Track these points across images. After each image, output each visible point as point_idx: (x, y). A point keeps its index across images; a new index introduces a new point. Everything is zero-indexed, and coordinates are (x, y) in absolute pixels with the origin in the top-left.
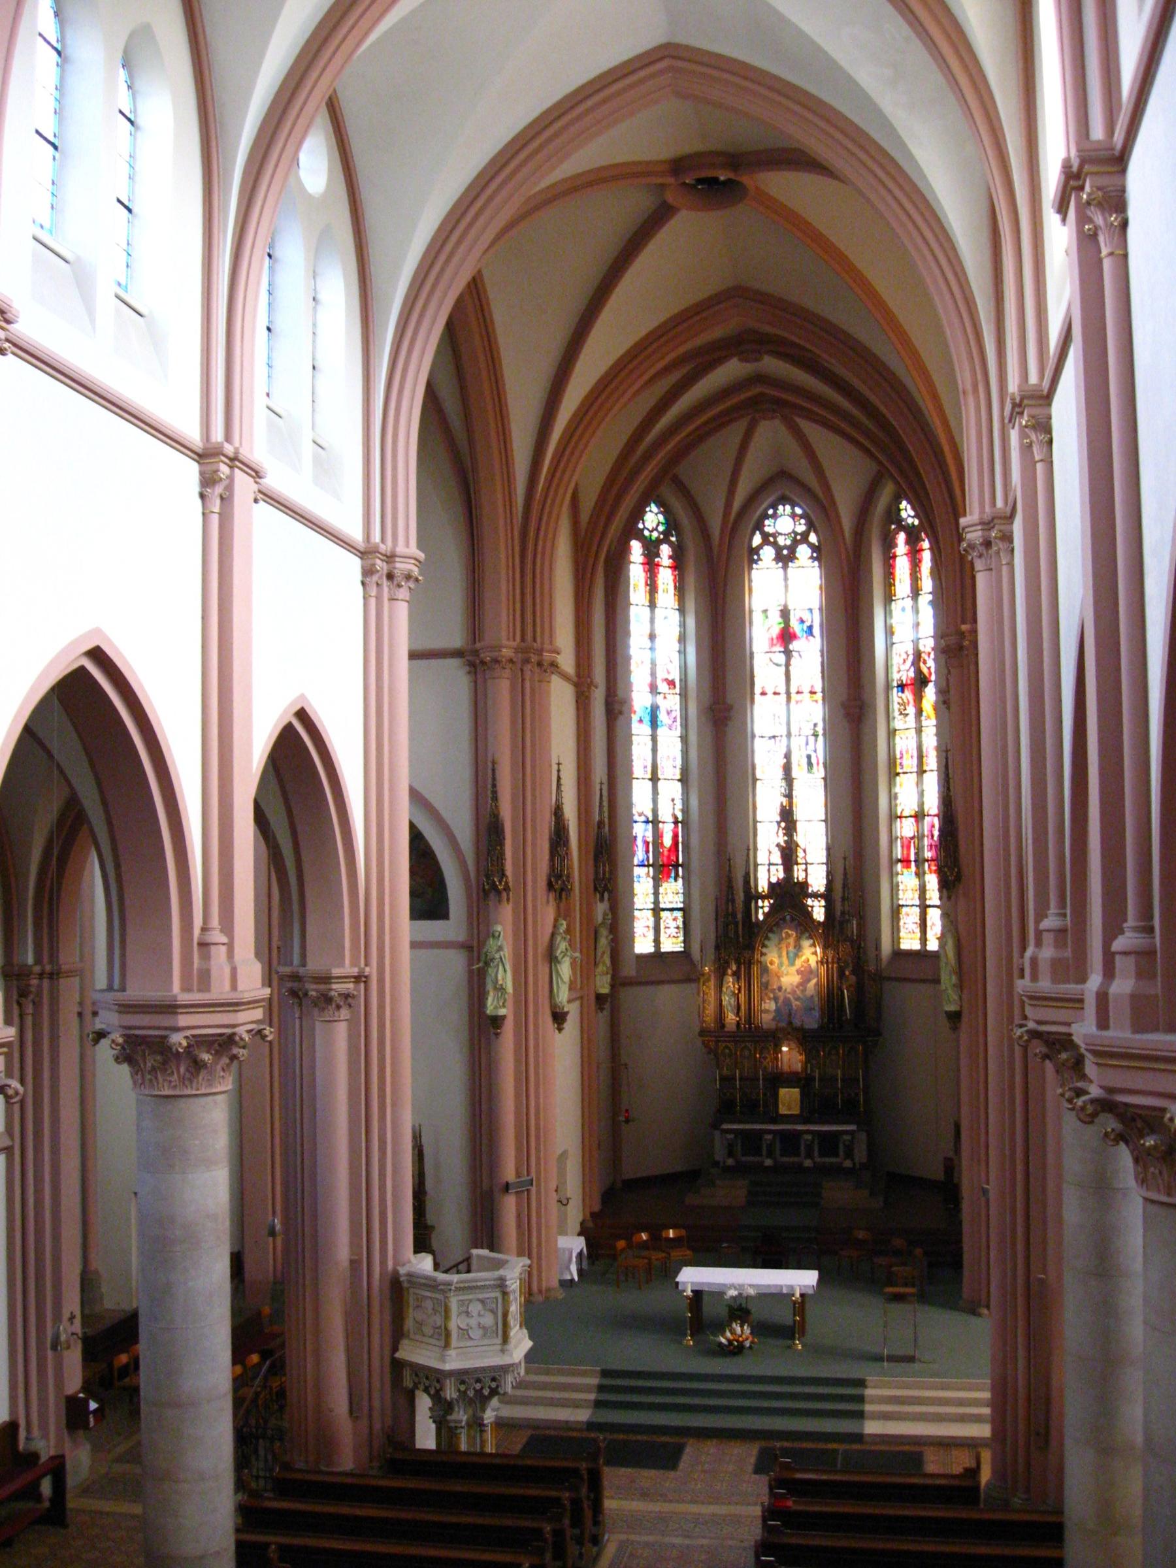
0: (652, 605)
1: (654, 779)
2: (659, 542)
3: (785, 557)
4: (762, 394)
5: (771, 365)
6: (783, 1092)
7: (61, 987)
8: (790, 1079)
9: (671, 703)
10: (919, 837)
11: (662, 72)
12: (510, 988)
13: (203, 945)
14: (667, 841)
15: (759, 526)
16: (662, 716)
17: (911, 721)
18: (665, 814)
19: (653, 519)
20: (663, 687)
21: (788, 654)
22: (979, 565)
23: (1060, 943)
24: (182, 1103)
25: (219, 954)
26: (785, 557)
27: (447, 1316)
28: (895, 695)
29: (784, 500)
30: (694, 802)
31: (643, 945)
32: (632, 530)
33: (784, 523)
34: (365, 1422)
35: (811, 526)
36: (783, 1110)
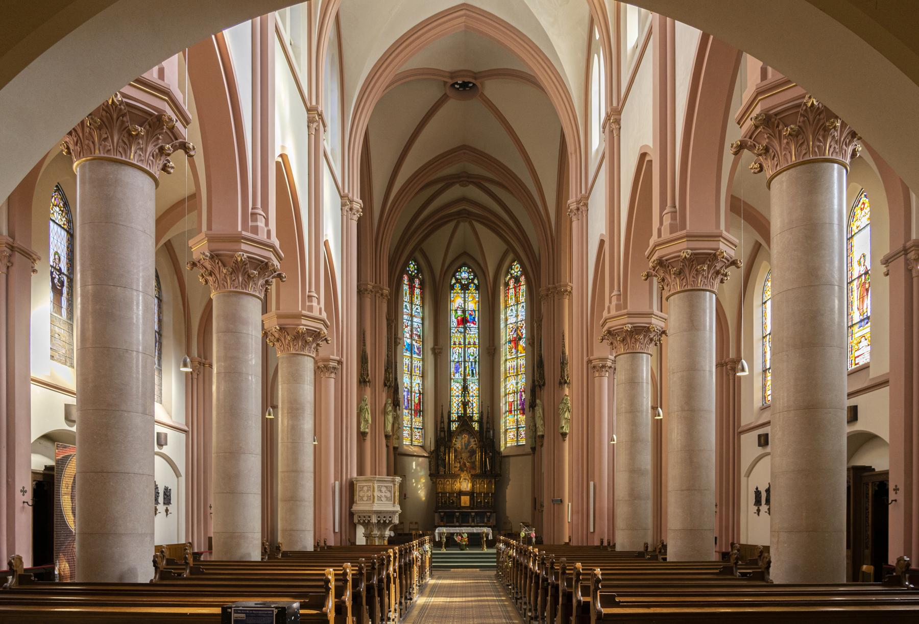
3: (465, 288)
4: (465, 209)
5: (473, 192)
6: (462, 497)
8: (465, 493)
11: (462, 16)
12: (370, 421)
13: (309, 297)
15: (454, 275)
18: (416, 388)
19: (412, 267)
22: (574, 219)
24: (300, 357)
26: (465, 288)
29: (465, 265)
32: (404, 271)
35: (475, 276)
36: (462, 505)
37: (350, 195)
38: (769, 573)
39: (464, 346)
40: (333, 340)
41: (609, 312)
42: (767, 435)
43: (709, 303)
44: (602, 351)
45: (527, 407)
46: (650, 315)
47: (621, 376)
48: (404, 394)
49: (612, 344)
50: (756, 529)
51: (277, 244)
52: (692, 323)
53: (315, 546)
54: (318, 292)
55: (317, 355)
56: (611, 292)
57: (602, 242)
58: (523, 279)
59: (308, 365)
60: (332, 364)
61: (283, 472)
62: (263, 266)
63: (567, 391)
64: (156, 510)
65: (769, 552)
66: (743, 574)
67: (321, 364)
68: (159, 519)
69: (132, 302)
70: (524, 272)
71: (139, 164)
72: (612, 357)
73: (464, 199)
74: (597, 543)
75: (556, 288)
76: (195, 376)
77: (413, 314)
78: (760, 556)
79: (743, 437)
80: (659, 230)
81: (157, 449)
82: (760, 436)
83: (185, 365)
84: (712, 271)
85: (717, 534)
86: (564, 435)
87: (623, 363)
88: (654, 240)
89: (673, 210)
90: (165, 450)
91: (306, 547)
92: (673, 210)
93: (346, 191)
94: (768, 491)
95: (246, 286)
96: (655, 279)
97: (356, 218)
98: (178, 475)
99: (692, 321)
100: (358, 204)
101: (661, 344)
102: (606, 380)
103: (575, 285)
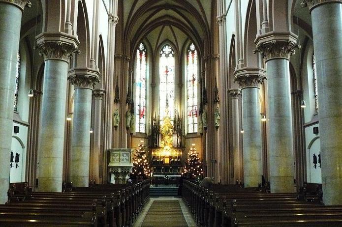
0: (141, 63)
1: (140, 97)
2: (142, 51)
3: (167, 56)
4: (167, 20)
5: (171, 12)
7: (62, 66)
9: (143, 83)
10: (193, 110)
12: (119, 121)
13: (91, 61)
14: (142, 110)
15: (162, 50)
16: (142, 85)
17: (192, 88)
19: (141, 46)
20: (142, 79)
21: (167, 75)
22: (219, 24)
23: (242, 62)
25: (94, 62)
26: (167, 56)
27: (120, 156)
28: (189, 82)
29: (167, 45)
30: (148, 103)
31: (137, 130)
32: (137, 48)
33: (167, 49)
34: (101, 179)
35: (172, 50)
37: (113, 15)
38: (322, 200)
39: (167, 85)
40: (102, 81)
41: (238, 68)
42: (318, 127)
43: (286, 65)
44: (235, 86)
45: (198, 114)
46: (257, 69)
47: (244, 99)
48: (137, 108)
49: (239, 83)
50: (315, 176)
51: (77, 37)
52: (278, 74)
53: (89, 185)
54: (95, 58)
55: (94, 88)
56: (238, 58)
57: (233, 36)
58: (196, 51)
59: (89, 93)
60: (101, 93)
61: (340, 58)
62: (70, 48)
63: (218, 106)
64: (11, 165)
65: (321, 188)
66: (309, 200)
67: (95, 92)
68: (13, 169)
69: (7, 65)
70: (196, 48)
71: (15, 4)
72: (240, 90)
73: (167, 16)
74: (235, 183)
75: (211, 56)
76: (35, 99)
77: (142, 68)
78: (317, 191)
79: (306, 128)
80: (260, 31)
81: (13, 134)
82: (314, 128)
83: (31, 93)
84: (286, 50)
85: (295, 178)
86: (217, 127)
87: (244, 93)
88: (258, 35)
89: (266, 22)
90: (18, 135)
91: (85, 185)
92: (266, 22)
93: (111, 13)
94: (319, 156)
95: (61, 57)
96: (260, 53)
97: (115, 24)
98: (23, 147)
99: (278, 73)
100: (116, 18)
101: (264, 84)
102: (237, 100)
103: (221, 55)
